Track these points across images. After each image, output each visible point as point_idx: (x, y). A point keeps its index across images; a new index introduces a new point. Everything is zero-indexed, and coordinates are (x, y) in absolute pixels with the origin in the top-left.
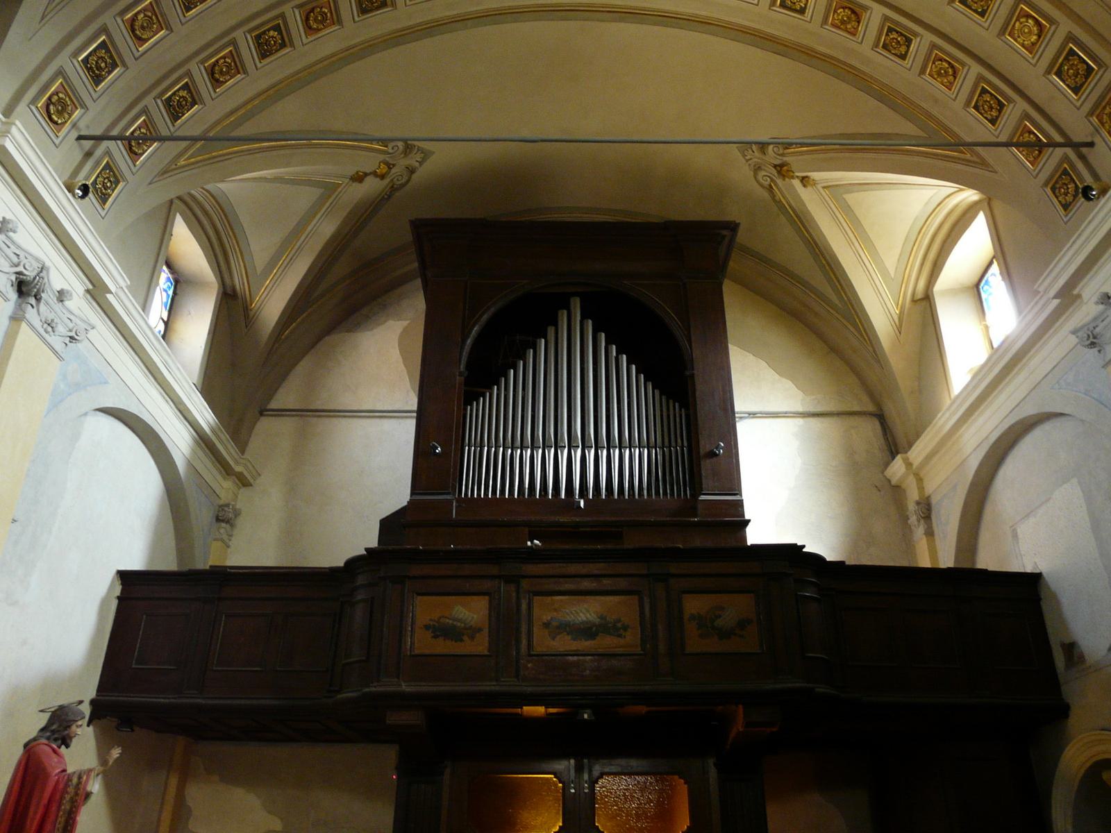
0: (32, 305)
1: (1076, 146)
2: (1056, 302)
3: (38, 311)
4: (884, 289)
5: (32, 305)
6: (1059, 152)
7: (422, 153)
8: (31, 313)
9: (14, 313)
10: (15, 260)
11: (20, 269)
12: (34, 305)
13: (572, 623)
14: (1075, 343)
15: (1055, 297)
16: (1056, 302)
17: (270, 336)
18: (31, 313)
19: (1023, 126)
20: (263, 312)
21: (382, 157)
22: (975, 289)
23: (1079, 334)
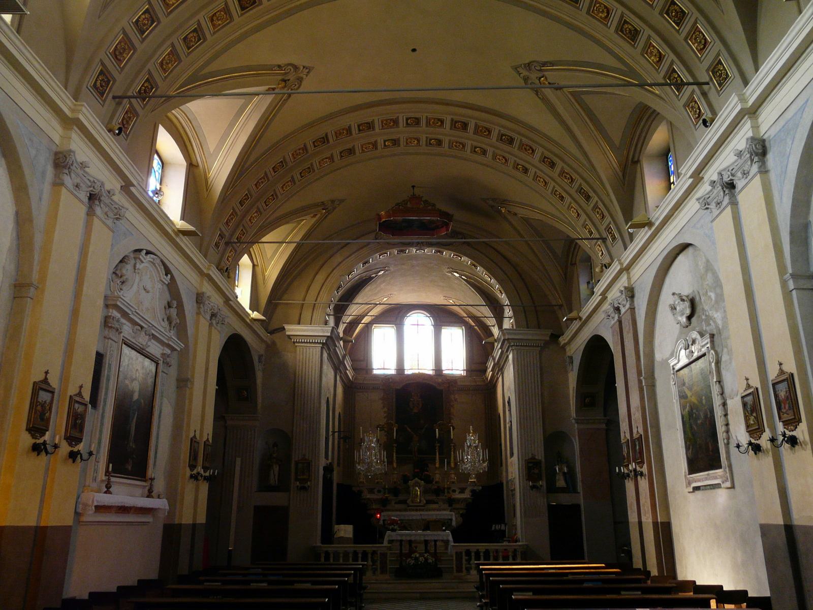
0: (67, 174)
1: (699, 84)
2: (691, 180)
3: (101, 207)
4: (611, 155)
5: (67, 174)
6: (691, 88)
7: (307, 68)
8: (98, 211)
9: (88, 211)
10: (90, 184)
11: (212, 311)
12: (68, 173)
13: (391, 380)
14: (699, 208)
15: (690, 177)
16: (691, 180)
17: (217, 202)
18: (67, 180)
19: (671, 69)
20: (212, 189)
21: (280, 78)
22: (665, 157)
23: (701, 201)
